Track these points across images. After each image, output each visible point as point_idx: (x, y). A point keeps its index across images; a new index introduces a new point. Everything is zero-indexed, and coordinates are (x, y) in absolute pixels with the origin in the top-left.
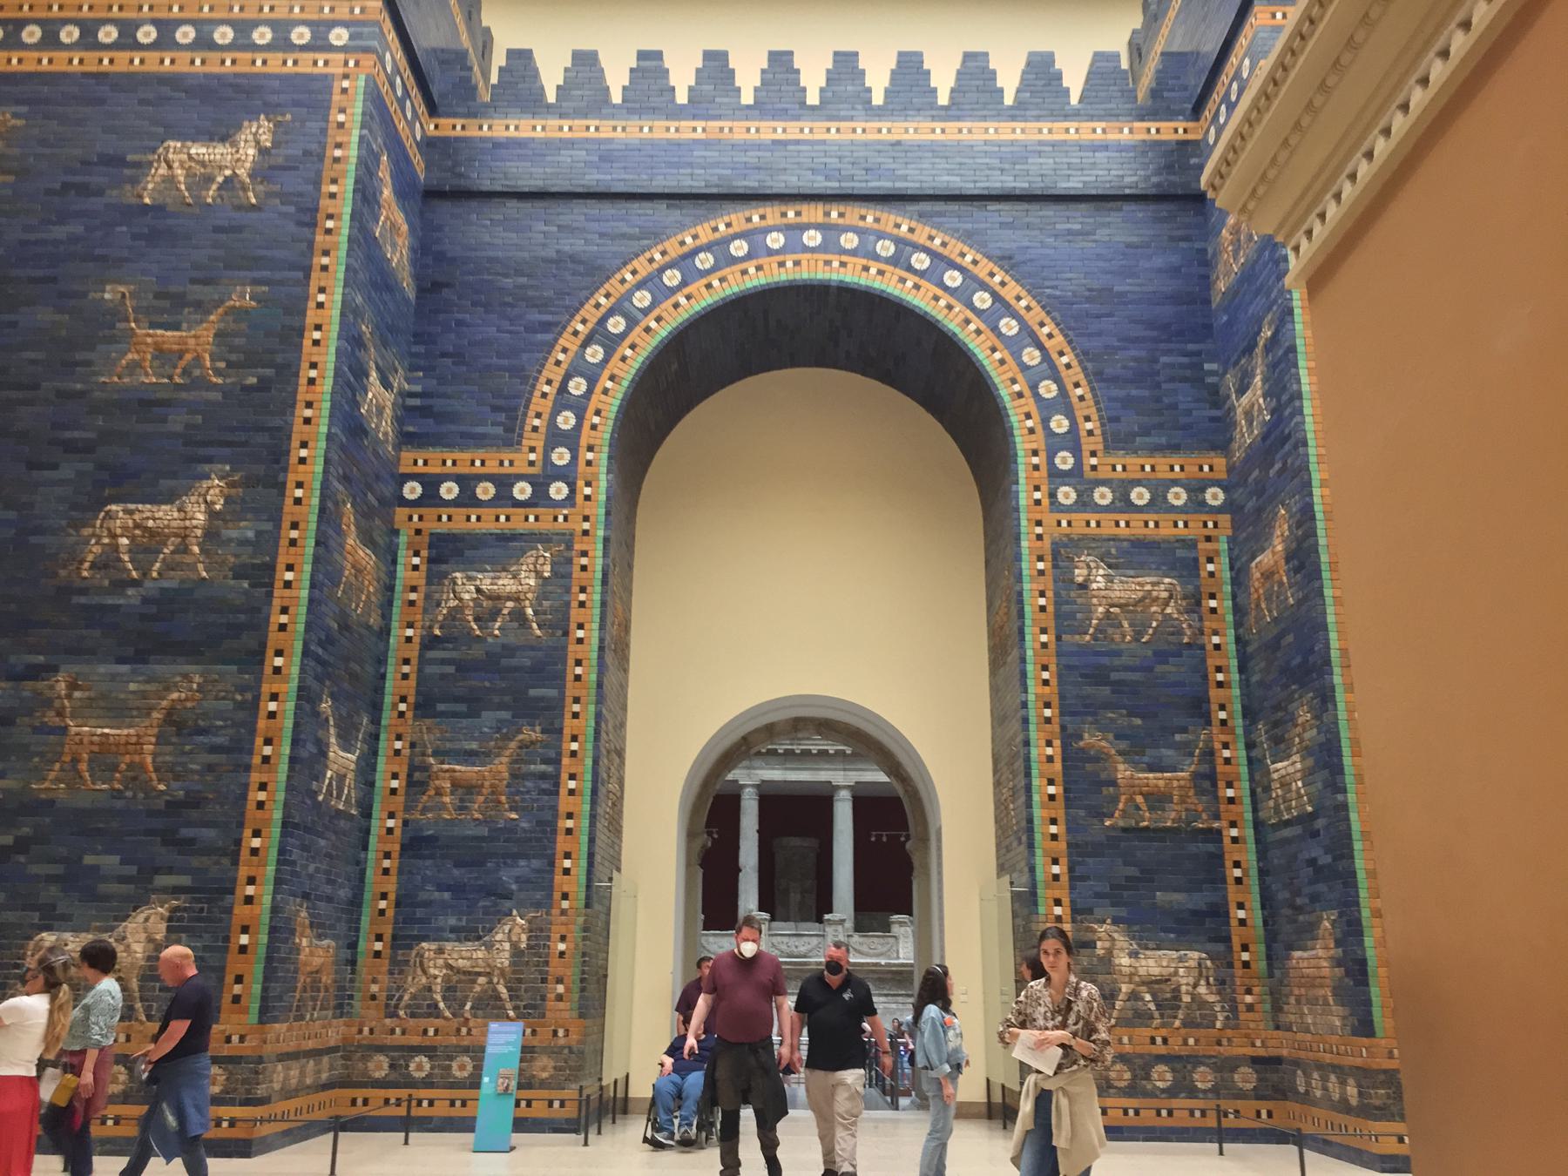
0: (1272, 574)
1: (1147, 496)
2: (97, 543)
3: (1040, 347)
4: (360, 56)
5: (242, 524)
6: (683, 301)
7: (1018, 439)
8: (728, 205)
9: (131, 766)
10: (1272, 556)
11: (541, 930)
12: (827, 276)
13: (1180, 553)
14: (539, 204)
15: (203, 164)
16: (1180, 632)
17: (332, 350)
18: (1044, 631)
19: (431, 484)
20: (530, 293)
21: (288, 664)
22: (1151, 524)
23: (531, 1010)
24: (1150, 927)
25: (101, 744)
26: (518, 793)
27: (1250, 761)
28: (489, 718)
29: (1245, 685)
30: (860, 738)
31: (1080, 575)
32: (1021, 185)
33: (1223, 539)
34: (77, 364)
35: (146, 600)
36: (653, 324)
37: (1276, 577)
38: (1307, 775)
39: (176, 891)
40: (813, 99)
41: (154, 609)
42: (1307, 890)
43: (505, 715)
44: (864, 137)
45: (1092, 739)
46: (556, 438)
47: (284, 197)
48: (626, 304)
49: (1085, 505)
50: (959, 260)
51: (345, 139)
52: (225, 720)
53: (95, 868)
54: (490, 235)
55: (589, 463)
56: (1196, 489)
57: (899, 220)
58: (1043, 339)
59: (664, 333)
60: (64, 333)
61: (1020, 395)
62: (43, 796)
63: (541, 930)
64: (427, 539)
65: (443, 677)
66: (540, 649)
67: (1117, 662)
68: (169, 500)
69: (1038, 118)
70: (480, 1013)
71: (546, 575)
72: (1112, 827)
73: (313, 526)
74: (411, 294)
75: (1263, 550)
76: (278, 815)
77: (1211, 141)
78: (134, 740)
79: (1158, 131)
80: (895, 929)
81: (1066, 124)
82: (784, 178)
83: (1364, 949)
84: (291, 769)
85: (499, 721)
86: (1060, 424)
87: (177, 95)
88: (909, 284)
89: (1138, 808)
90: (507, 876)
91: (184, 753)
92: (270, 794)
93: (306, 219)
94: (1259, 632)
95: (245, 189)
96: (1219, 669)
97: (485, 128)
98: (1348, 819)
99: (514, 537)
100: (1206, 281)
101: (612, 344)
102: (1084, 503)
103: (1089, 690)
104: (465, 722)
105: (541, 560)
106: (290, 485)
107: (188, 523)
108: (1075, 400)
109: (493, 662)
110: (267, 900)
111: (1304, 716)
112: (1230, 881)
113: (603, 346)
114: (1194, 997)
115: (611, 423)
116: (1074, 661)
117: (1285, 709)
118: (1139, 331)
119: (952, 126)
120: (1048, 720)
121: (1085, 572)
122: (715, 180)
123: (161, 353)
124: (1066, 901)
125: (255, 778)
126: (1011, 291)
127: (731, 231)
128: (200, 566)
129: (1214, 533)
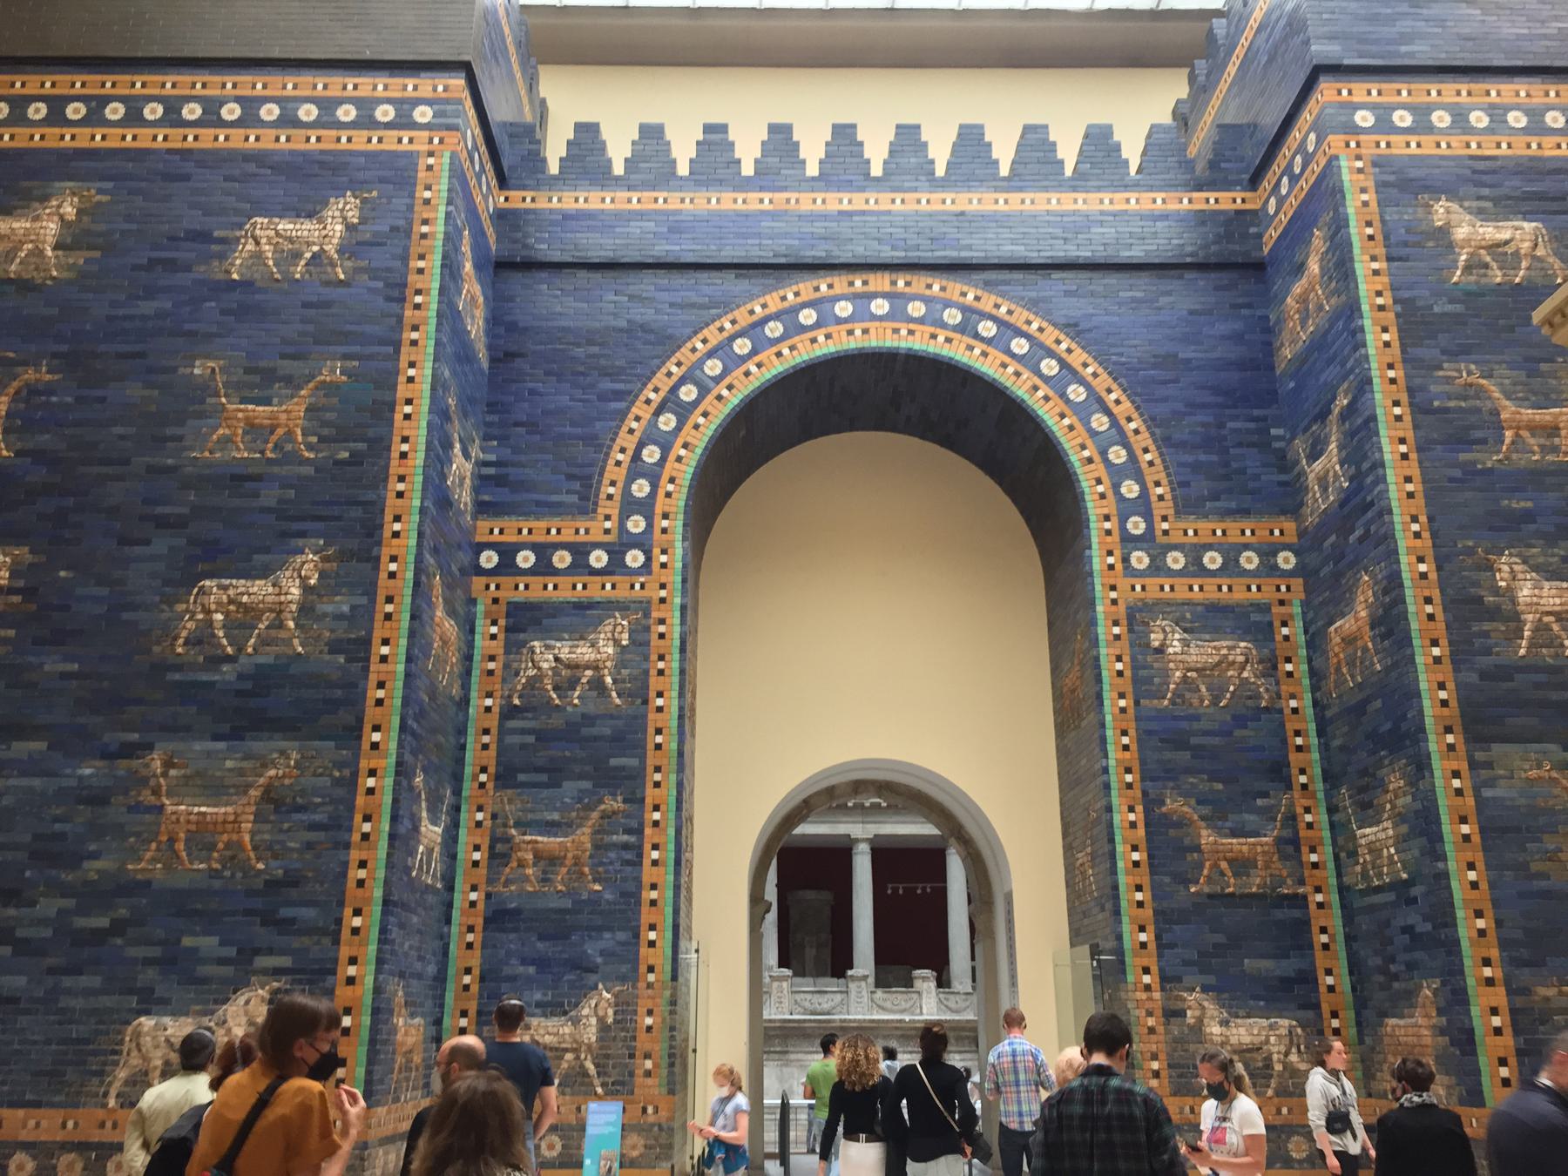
0: (1355, 639)
1: (1220, 560)
2: (190, 619)
3: (1109, 413)
4: (444, 133)
5: (338, 598)
6: (754, 369)
7: (1090, 505)
8: (796, 275)
9: (228, 845)
10: (1355, 620)
11: (628, 1004)
12: (895, 344)
13: (1255, 617)
14: (610, 274)
15: (290, 240)
16: (1258, 697)
17: (424, 424)
18: (1122, 696)
19: (508, 553)
20: (603, 362)
21: (386, 739)
22: (1225, 588)
23: (620, 1087)
24: (1241, 995)
25: (197, 823)
26: (602, 864)
27: (1332, 826)
28: (570, 787)
29: (1324, 748)
30: (898, 793)
31: (1155, 639)
32: (1085, 254)
33: (1297, 602)
34: (166, 439)
35: (241, 677)
36: (725, 393)
37: (1360, 643)
38: (1401, 842)
39: (277, 972)
40: (876, 170)
41: (249, 685)
42: (1403, 957)
43: (586, 785)
44: (928, 208)
45: (1173, 805)
46: (631, 505)
47: (374, 274)
48: (698, 372)
49: (1158, 569)
50: (1025, 328)
51: (431, 215)
52: (323, 797)
53: (195, 950)
54: (555, 304)
55: (664, 531)
56: (1268, 553)
57: (965, 288)
58: (1111, 405)
59: (736, 401)
60: (153, 408)
61: (1090, 460)
62: (139, 877)
63: (628, 1004)
64: (504, 608)
65: (523, 746)
66: (618, 718)
67: (1196, 726)
68: (264, 575)
69: (1099, 189)
70: (568, 1090)
71: (624, 643)
72: (1197, 893)
73: (408, 600)
74: (485, 365)
75: (1343, 615)
76: (378, 893)
77: (1271, 211)
78: (231, 818)
79: (1217, 201)
80: (918, 984)
81: (1127, 195)
82: (850, 247)
83: (1471, 1019)
84: (391, 845)
85: (580, 791)
86: (1130, 489)
87: (262, 171)
88: (977, 351)
89: (1222, 874)
90: (592, 949)
91: (281, 831)
92: (369, 873)
93: (396, 294)
94: (1340, 697)
95: (334, 265)
96: (1297, 733)
97: (555, 199)
98: (1449, 887)
99: (592, 605)
100: (1269, 349)
101: (684, 412)
102: (1157, 568)
103: (1168, 755)
104: (545, 793)
105: (619, 629)
106: (385, 558)
107: (283, 598)
108: (1144, 466)
109: (573, 731)
110: (369, 980)
111: (1396, 782)
112: (1317, 947)
113: (676, 413)
114: (1286, 1065)
115: (685, 490)
116: (1153, 726)
117: (1374, 775)
118: (1208, 398)
119: (1015, 197)
120: (1129, 786)
121: (1161, 636)
122: (783, 250)
123: (252, 427)
124: (1154, 969)
125: (355, 855)
126: (1078, 358)
127: (799, 300)
128: (296, 642)
129: (1287, 597)
